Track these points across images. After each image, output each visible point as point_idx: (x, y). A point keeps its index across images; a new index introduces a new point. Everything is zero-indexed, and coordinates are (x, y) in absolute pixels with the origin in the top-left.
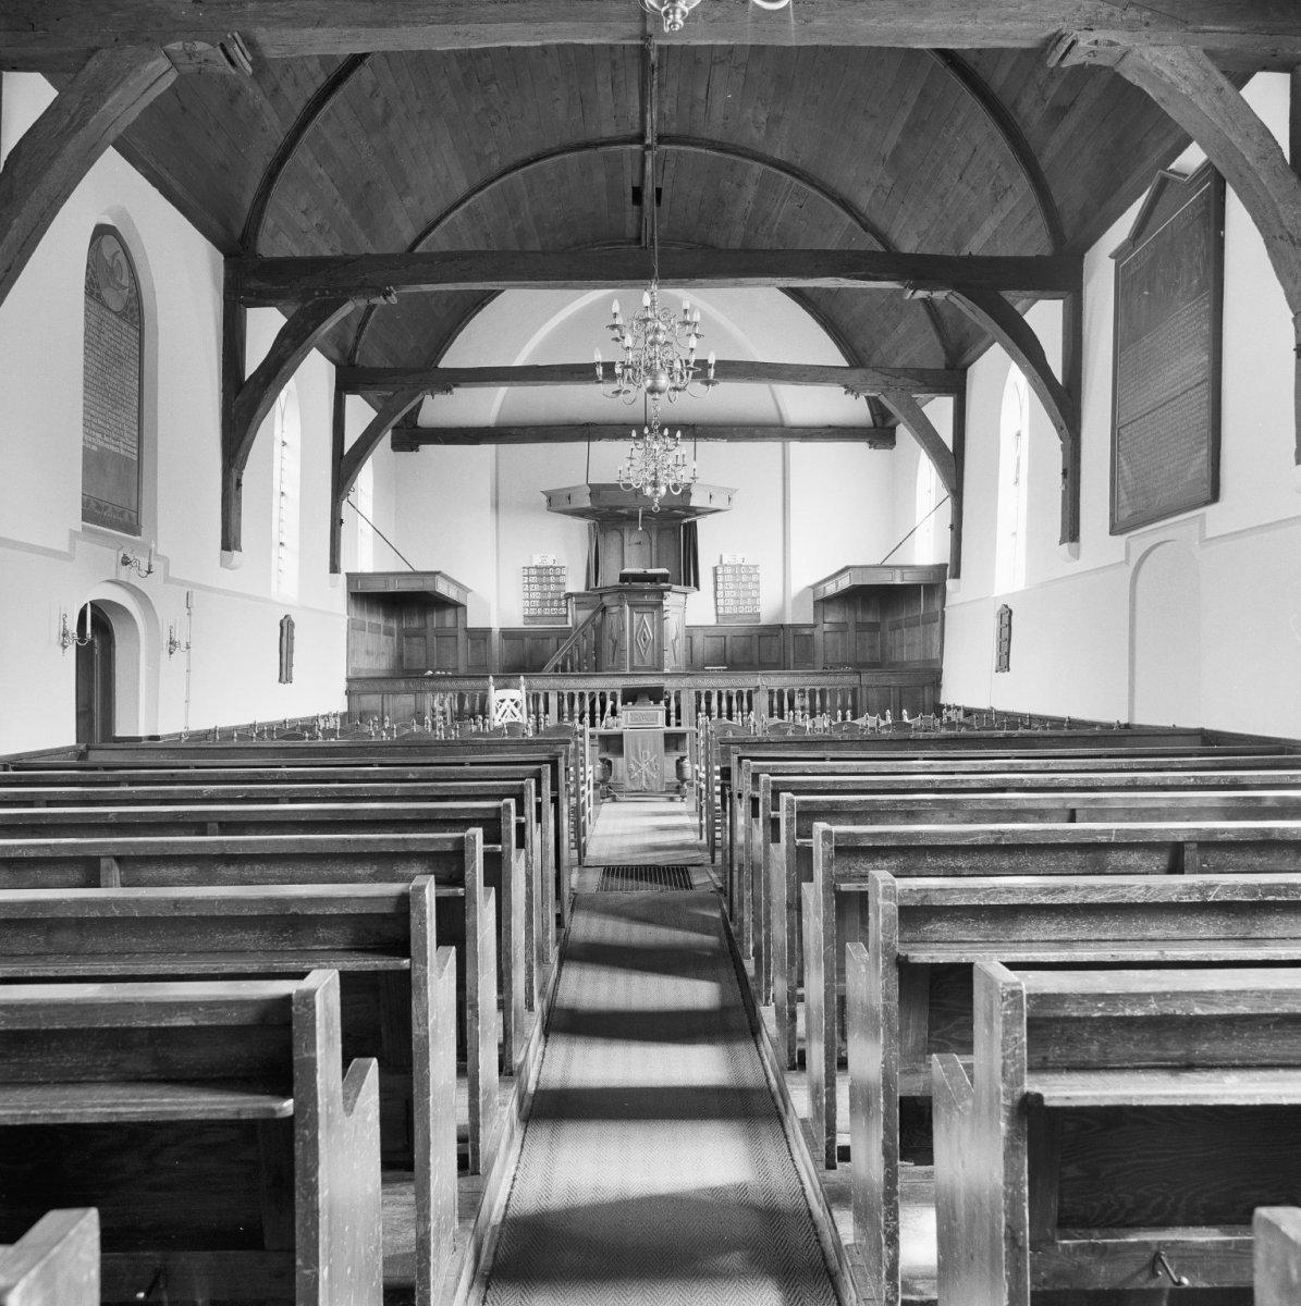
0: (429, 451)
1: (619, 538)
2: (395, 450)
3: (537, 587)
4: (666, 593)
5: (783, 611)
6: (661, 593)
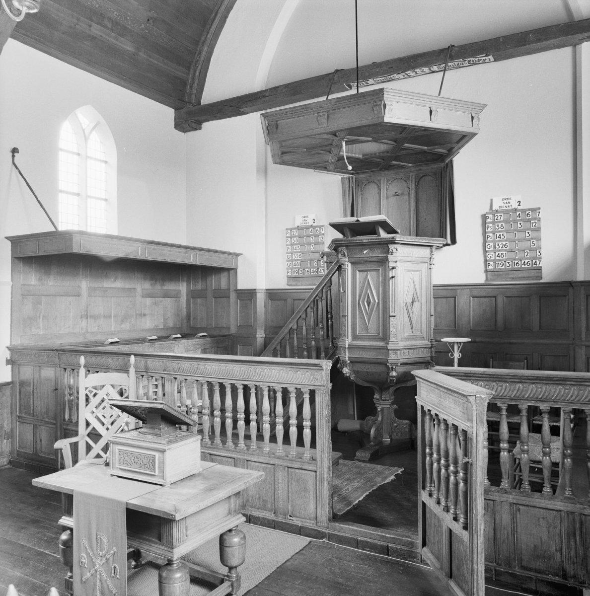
0: (211, 127)
1: (377, 191)
2: (184, 130)
3: (297, 248)
4: (391, 247)
5: (572, 265)
6: (385, 245)
